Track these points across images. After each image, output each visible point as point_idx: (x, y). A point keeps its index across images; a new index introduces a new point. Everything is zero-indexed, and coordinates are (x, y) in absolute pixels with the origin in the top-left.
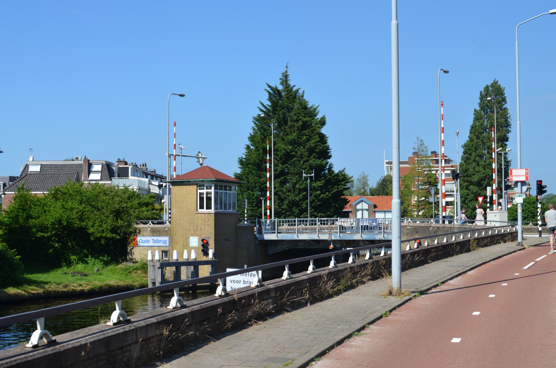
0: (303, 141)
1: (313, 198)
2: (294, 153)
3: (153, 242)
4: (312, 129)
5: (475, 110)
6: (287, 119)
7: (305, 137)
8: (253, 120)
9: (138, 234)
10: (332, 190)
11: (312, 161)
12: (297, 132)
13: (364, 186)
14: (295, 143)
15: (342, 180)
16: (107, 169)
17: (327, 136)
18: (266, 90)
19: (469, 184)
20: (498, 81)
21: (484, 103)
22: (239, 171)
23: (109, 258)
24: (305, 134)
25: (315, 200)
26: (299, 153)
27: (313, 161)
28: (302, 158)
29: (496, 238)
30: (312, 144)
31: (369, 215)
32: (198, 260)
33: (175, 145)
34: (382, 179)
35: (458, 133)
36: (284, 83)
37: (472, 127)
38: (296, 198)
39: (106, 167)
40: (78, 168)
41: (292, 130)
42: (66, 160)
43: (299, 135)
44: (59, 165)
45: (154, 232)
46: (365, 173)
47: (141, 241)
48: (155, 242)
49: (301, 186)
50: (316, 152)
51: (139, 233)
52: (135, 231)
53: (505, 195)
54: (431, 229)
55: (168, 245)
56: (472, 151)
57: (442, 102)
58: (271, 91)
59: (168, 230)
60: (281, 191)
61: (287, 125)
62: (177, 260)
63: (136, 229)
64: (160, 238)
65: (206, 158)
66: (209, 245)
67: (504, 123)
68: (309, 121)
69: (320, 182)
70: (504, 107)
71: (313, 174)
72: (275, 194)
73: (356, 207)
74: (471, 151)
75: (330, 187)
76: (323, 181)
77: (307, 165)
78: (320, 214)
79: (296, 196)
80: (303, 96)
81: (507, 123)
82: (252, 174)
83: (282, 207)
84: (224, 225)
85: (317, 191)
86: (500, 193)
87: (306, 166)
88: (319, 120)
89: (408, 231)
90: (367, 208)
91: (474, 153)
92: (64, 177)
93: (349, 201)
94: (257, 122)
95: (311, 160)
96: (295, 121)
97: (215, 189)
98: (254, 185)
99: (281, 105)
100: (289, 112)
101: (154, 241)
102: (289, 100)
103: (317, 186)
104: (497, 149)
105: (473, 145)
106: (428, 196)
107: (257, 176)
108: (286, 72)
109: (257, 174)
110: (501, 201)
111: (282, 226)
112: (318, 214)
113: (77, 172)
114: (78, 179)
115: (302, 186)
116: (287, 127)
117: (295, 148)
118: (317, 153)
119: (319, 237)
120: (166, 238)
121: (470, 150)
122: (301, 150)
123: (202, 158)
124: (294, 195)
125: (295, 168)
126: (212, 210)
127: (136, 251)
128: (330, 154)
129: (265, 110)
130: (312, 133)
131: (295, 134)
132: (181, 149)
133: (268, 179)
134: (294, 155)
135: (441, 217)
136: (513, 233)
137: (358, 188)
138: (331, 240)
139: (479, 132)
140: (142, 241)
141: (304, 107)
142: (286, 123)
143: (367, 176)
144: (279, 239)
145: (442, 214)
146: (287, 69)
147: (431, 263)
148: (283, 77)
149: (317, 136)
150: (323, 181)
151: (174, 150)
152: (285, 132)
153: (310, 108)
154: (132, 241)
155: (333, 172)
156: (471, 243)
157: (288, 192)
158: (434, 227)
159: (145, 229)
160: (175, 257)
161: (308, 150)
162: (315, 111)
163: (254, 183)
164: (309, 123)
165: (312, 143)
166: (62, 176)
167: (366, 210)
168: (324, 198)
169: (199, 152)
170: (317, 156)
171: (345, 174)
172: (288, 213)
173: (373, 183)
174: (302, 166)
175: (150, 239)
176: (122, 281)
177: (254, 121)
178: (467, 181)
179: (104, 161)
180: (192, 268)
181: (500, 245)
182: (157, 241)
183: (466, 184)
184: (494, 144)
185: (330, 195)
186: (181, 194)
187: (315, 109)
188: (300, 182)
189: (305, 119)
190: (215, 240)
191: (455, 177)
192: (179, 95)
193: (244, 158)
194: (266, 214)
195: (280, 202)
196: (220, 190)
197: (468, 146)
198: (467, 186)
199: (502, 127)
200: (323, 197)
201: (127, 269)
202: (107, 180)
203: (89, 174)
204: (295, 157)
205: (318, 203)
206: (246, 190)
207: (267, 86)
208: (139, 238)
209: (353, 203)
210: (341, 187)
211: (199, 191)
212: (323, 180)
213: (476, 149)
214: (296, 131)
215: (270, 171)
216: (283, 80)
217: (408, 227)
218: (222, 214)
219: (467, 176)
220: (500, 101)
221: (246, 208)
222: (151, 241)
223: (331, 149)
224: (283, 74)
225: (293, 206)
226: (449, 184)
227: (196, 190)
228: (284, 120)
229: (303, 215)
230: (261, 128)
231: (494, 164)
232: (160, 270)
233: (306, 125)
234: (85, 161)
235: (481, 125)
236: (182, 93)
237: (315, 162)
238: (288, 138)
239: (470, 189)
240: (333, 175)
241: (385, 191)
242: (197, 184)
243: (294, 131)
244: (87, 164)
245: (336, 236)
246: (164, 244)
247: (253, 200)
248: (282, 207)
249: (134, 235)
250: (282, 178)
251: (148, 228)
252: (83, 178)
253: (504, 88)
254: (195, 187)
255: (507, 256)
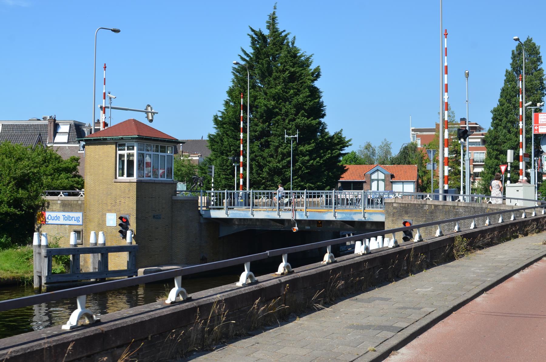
0: (289, 96)
1: (299, 165)
2: (277, 110)
3: (64, 219)
4: (301, 81)
5: (507, 71)
6: (272, 70)
7: (292, 91)
8: (233, 71)
9: (46, 209)
10: (325, 155)
11: (299, 120)
12: (283, 84)
13: (386, 154)
14: (279, 98)
15: (338, 144)
16: (75, 131)
17: (321, 90)
18: (249, 35)
19: (499, 153)
20: (531, 39)
21: (517, 64)
22: (214, 131)
23: (10, 239)
24: (293, 87)
25: (302, 167)
26: (284, 110)
27: (301, 120)
28: (287, 116)
29: (510, 229)
30: (300, 100)
31: (385, 186)
32: (108, 244)
33: (105, 93)
34: (404, 146)
35: (468, 74)
36: (271, 27)
37: (503, 90)
38: (279, 165)
39: (74, 128)
40: (43, 129)
41: (277, 82)
42: (30, 120)
43: (285, 88)
44: (23, 125)
45: (66, 207)
46: (387, 140)
47: (50, 218)
48: (66, 219)
49: (284, 149)
50: (304, 109)
51: (48, 207)
52: (44, 204)
53: (535, 163)
54: (426, 207)
55: (81, 223)
56: (503, 117)
57: (446, 30)
58: (254, 36)
59: (81, 204)
60: (260, 156)
61: (271, 77)
62: (104, 244)
63: (44, 202)
64: (72, 214)
65: (157, 113)
66: (129, 225)
67: (538, 86)
68: (298, 72)
69: (309, 146)
70: (539, 67)
71: (297, 135)
72: (251, 160)
73: (371, 177)
74: (501, 117)
75: (322, 151)
76: (313, 145)
77: (293, 125)
78: (308, 185)
79: (279, 162)
80: (293, 44)
81: (542, 86)
82: (227, 135)
83: (261, 176)
84: (152, 198)
85: (305, 156)
86: (528, 161)
87: (292, 126)
88: (312, 71)
89: (395, 211)
90: (383, 178)
91: (504, 119)
92: (24, 139)
93: (348, 169)
94: (238, 74)
95: (298, 118)
96: (280, 71)
97: (138, 149)
98: (228, 148)
99: (265, 53)
100: (275, 61)
101: (65, 218)
102: (276, 47)
103: (305, 150)
104: (526, 103)
105: (503, 110)
106: (454, 165)
107: (234, 138)
108: (274, 13)
109: (233, 135)
110: (529, 170)
111: (259, 199)
112: (306, 184)
113: (39, 133)
114: (40, 141)
115: (285, 150)
116: (271, 79)
117: (280, 104)
118: (306, 111)
119: (280, 216)
120: (79, 215)
121: (500, 115)
122: (287, 107)
123: (152, 113)
124: (277, 161)
125: (278, 128)
126: (134, 178)
127: (44, 230)
128: (323, 113)
129: (248, 59)
130: (302, 86)
131: (279, 87)
132: (110, 98)
133: (241, 141)
134: (277, 112)
135: (441, 191)
136: (541, 220)
137: (380, 156)
138: (296, 220)
139: (511, 96)
140: (51, 217)
141: (293, 55)
142: (270, 75)
143: (390, 143)
144: (230, 217)
145: (444, 187)
146: (275, 10)
147: (322, 309)
148: (270, 19)
149: (307, 89)
150: (313, 145)
151: (104, 100)
152: (269, 85)
153: (300, 57)
154: (39, 217)
155: (327, 134)
156: (456, 243)
157: (270, 157)
158: (430, 205)
159: (54, 202)
160: (92, 240)
161: (295, 106)
162: (308, 61)
163: (228, 146)
164: (298, 75)
165: (300, 98)
166: (23, 137)
167: (382, 180)
168: (314, 165)
169: (149, 106)
170: (306, 114)
171: (341, 137)
172: (268, 183)
173: (395, 152)
174: (287, 126)
175: (60, 214)
176: (9, 272)
177: (233, 72)
178: (497, 150)
179: (73, 121)
180: (99, 256)
181: (516, 240)
182: (69, 218)
183: (495, 153)
184: (522, 97)
185: (322, 161)
186: (97, 157)
187: (308, 59)
188: (283, 145)
189: (293, 70)
190: (137, 218)
191: (461, 135)
192: (112, 30)
193: (220, 117)
194: (238, 184)
195: (258, 170)
196: (160, 152)
197: (498, 110)
198: (497, 155)
199: (537, 90)
200: (313, 163)
201: (25, 255)
202: (74, 143)
203: (55, 136)
204: (279, 115)
205: (306, 171)
206: (219, 155)
207: (250, 30)
208: (47, 214)
209: (368, 173)
210: (336, 152)
211: (119, 152)
212: (313, 143)
213: (507, 114)
214: (282, 83)
215: (245, 131)
216: (270, 24)
217: (395, 205)
218: (149, 183)
219: (496, 144)
220: (535, 61)
221: (213, 175)
222: (62, 218)
223: (325, 106)
224: (270, 17)
225: (274, 175)
226: (478, 153)
227: (114, 151)
228: (267, 70)
229: (286, 185)
230: (242, 80)
231: (521, 122)
232: (46, 260)
233: (295, 77)
234: (50, 121)
235: (514, 87)
236: (116, 28)
237: (303, 121)
238: (271, 92)
239: (500, 159)
240: (326, 137)
241: (407, 160)
242: (116, 144)
243: (279, 83)
244: (52, 124)
245: (302, 215)
246: (76, 221)
247: (228, 166)
248: (261, 176)
249: (41, 209)
250: (263, 140)
251: (59, 200)
252: (48, 140)
253: (540, 46)
254: (114, 146)
255: (521, 273)
